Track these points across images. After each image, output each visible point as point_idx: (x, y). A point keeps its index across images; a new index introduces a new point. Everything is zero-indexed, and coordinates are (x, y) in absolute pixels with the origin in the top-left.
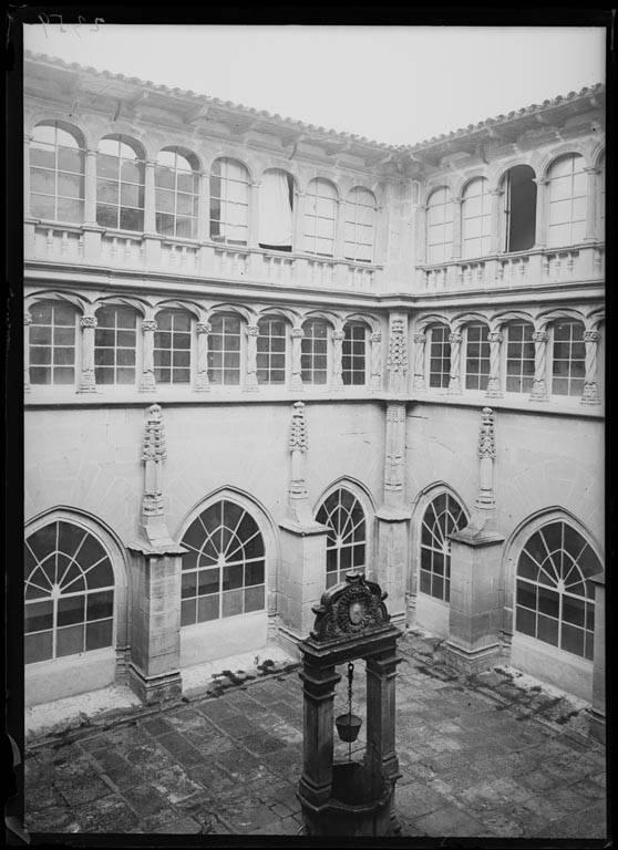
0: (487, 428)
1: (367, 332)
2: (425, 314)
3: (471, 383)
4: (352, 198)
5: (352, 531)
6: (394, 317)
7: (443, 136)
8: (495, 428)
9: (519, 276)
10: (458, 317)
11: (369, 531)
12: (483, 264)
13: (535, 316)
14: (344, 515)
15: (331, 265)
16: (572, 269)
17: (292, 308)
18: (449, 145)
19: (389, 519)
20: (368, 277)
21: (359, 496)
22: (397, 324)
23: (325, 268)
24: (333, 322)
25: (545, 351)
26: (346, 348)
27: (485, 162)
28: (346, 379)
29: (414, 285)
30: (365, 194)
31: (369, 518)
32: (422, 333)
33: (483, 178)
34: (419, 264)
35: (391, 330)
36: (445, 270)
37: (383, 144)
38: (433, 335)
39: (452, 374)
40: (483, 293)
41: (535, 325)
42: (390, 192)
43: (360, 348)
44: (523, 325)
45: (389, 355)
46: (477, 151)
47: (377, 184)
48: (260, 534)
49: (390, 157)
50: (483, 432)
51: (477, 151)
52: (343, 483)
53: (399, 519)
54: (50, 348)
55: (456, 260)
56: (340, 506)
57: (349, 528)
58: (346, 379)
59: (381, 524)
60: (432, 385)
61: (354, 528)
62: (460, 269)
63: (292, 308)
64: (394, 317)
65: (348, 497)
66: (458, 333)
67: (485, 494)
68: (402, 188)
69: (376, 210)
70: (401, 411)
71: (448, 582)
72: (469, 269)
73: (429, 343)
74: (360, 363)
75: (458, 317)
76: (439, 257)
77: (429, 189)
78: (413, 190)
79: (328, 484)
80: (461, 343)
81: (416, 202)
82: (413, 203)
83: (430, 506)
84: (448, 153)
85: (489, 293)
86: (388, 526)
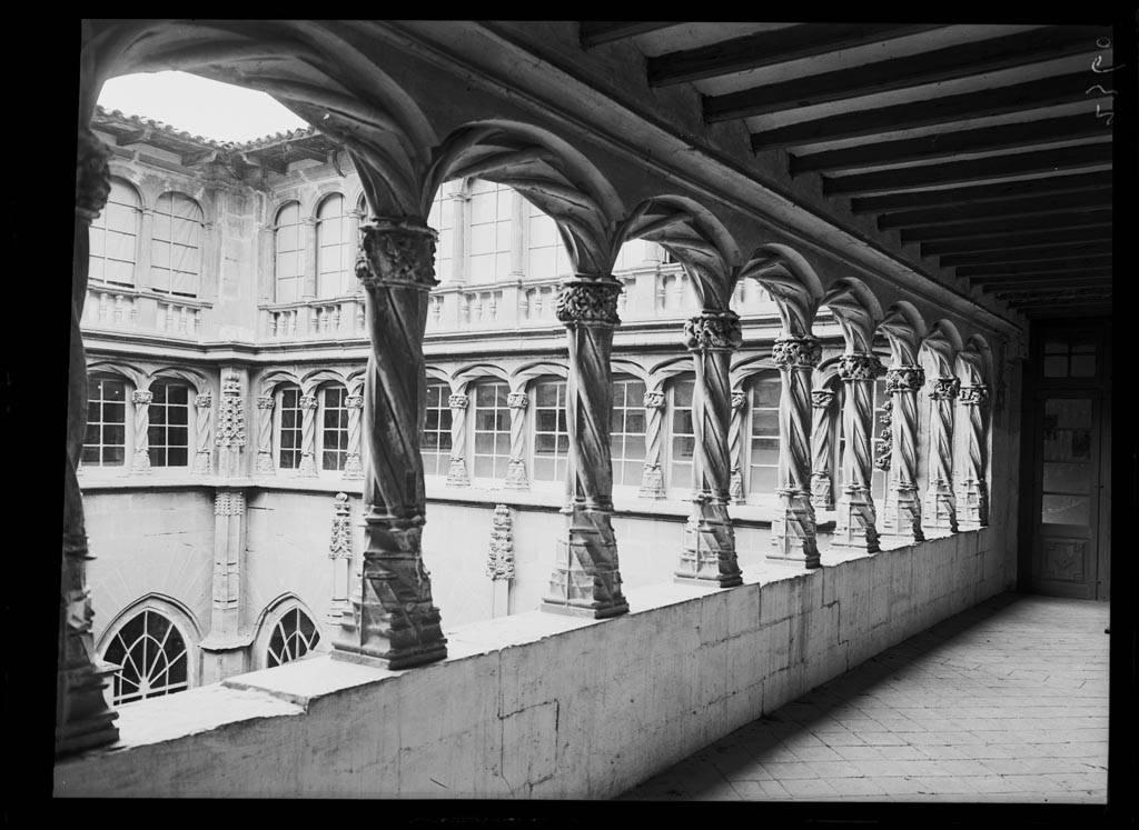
0: (342, 519)
1: (190, 394)
2: (271, 370)
3: (329, 462)
4: (165, 206)
5: (166, 669)
6: (227, 374)
7: (279, 135)
8: (516, 532)
9: (333, 328)
10: (311, 375)
11: (192, 668)
12: (499, 294)
13: (649, 369)
14: (152, 647)
15: (131, 299)
16: (495, 313)
17: (132, 364)
18: (289, 147)
19: (215, 648)
20: (191, 317)
21: (176, 620)
22: (230, 383)
23: (119, 301)
24: (134, 378)
25: (314, 418)
26: (155, 414)
27: (341, 174)
28: (157, 458)
29: (254, 331)
30: (187, 202)
31: (191, 649)
32: (268, 396)
33: (342, 196)
34: (263, 303)
35: (222, 391)
36: (339, 307)
37: (200, 138)
38: (284, 398)
39: (304, 450)
40: (335, 345)
41: (647, 381)
42: (223, 203)
43: (180, 416)
44: (496, 384)
45: (219, 425)
46: (330, 159)
47: (202, 189)
48: (174, 627)
49: (214, 156)
50: (336, 525)
51: (330, 159)
52: (149, 603)
53: (230, 647)
54: (554, 430)
55: (307, 300)
56: (145, 635)
57: (161, 665)
58: (157, 458)
59: (206, 655)
60: (283, 464)
61: (168, 666)
62: (314, 312)
63: (132, 364)
64: (227, 374)
65: (158, 623)
66: (311, 395)
67: (339, 605)
68: (241, 201)
69: (203, 226)
70: (237, 502)
71: (163, 693)
72: (538, 295)
73: (280, 409)
74: (180, 437)
75: (311, 375)
76: (292, 292)
77: (277, 202)
78: (256, 203)
79: (121, 608)
80: (316, 410)
81: (259, 219)
82: (256, 218)
83: (278, 626)
84: (296, 158)
85: (342, 345)
86: (216, 658)
